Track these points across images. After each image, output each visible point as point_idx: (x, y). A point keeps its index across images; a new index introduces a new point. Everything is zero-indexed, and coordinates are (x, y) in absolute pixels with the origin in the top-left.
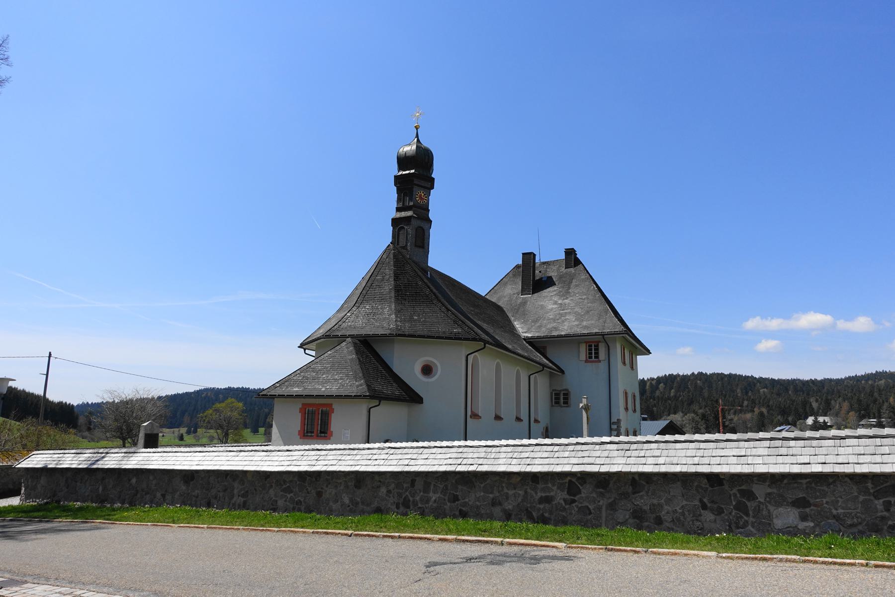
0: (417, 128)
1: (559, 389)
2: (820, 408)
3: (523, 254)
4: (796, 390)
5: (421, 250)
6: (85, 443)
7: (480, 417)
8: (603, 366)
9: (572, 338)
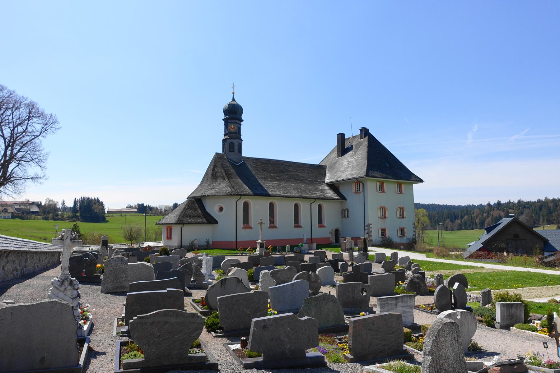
0: (233, 93)
1: (345, 209)
2: (462, 217)
3: (338, 135)
4: (447, 208)
5: (233, 153)
6: (545, 212)
7: (252, 228)
8: (362, 194)
9: (363, 178)
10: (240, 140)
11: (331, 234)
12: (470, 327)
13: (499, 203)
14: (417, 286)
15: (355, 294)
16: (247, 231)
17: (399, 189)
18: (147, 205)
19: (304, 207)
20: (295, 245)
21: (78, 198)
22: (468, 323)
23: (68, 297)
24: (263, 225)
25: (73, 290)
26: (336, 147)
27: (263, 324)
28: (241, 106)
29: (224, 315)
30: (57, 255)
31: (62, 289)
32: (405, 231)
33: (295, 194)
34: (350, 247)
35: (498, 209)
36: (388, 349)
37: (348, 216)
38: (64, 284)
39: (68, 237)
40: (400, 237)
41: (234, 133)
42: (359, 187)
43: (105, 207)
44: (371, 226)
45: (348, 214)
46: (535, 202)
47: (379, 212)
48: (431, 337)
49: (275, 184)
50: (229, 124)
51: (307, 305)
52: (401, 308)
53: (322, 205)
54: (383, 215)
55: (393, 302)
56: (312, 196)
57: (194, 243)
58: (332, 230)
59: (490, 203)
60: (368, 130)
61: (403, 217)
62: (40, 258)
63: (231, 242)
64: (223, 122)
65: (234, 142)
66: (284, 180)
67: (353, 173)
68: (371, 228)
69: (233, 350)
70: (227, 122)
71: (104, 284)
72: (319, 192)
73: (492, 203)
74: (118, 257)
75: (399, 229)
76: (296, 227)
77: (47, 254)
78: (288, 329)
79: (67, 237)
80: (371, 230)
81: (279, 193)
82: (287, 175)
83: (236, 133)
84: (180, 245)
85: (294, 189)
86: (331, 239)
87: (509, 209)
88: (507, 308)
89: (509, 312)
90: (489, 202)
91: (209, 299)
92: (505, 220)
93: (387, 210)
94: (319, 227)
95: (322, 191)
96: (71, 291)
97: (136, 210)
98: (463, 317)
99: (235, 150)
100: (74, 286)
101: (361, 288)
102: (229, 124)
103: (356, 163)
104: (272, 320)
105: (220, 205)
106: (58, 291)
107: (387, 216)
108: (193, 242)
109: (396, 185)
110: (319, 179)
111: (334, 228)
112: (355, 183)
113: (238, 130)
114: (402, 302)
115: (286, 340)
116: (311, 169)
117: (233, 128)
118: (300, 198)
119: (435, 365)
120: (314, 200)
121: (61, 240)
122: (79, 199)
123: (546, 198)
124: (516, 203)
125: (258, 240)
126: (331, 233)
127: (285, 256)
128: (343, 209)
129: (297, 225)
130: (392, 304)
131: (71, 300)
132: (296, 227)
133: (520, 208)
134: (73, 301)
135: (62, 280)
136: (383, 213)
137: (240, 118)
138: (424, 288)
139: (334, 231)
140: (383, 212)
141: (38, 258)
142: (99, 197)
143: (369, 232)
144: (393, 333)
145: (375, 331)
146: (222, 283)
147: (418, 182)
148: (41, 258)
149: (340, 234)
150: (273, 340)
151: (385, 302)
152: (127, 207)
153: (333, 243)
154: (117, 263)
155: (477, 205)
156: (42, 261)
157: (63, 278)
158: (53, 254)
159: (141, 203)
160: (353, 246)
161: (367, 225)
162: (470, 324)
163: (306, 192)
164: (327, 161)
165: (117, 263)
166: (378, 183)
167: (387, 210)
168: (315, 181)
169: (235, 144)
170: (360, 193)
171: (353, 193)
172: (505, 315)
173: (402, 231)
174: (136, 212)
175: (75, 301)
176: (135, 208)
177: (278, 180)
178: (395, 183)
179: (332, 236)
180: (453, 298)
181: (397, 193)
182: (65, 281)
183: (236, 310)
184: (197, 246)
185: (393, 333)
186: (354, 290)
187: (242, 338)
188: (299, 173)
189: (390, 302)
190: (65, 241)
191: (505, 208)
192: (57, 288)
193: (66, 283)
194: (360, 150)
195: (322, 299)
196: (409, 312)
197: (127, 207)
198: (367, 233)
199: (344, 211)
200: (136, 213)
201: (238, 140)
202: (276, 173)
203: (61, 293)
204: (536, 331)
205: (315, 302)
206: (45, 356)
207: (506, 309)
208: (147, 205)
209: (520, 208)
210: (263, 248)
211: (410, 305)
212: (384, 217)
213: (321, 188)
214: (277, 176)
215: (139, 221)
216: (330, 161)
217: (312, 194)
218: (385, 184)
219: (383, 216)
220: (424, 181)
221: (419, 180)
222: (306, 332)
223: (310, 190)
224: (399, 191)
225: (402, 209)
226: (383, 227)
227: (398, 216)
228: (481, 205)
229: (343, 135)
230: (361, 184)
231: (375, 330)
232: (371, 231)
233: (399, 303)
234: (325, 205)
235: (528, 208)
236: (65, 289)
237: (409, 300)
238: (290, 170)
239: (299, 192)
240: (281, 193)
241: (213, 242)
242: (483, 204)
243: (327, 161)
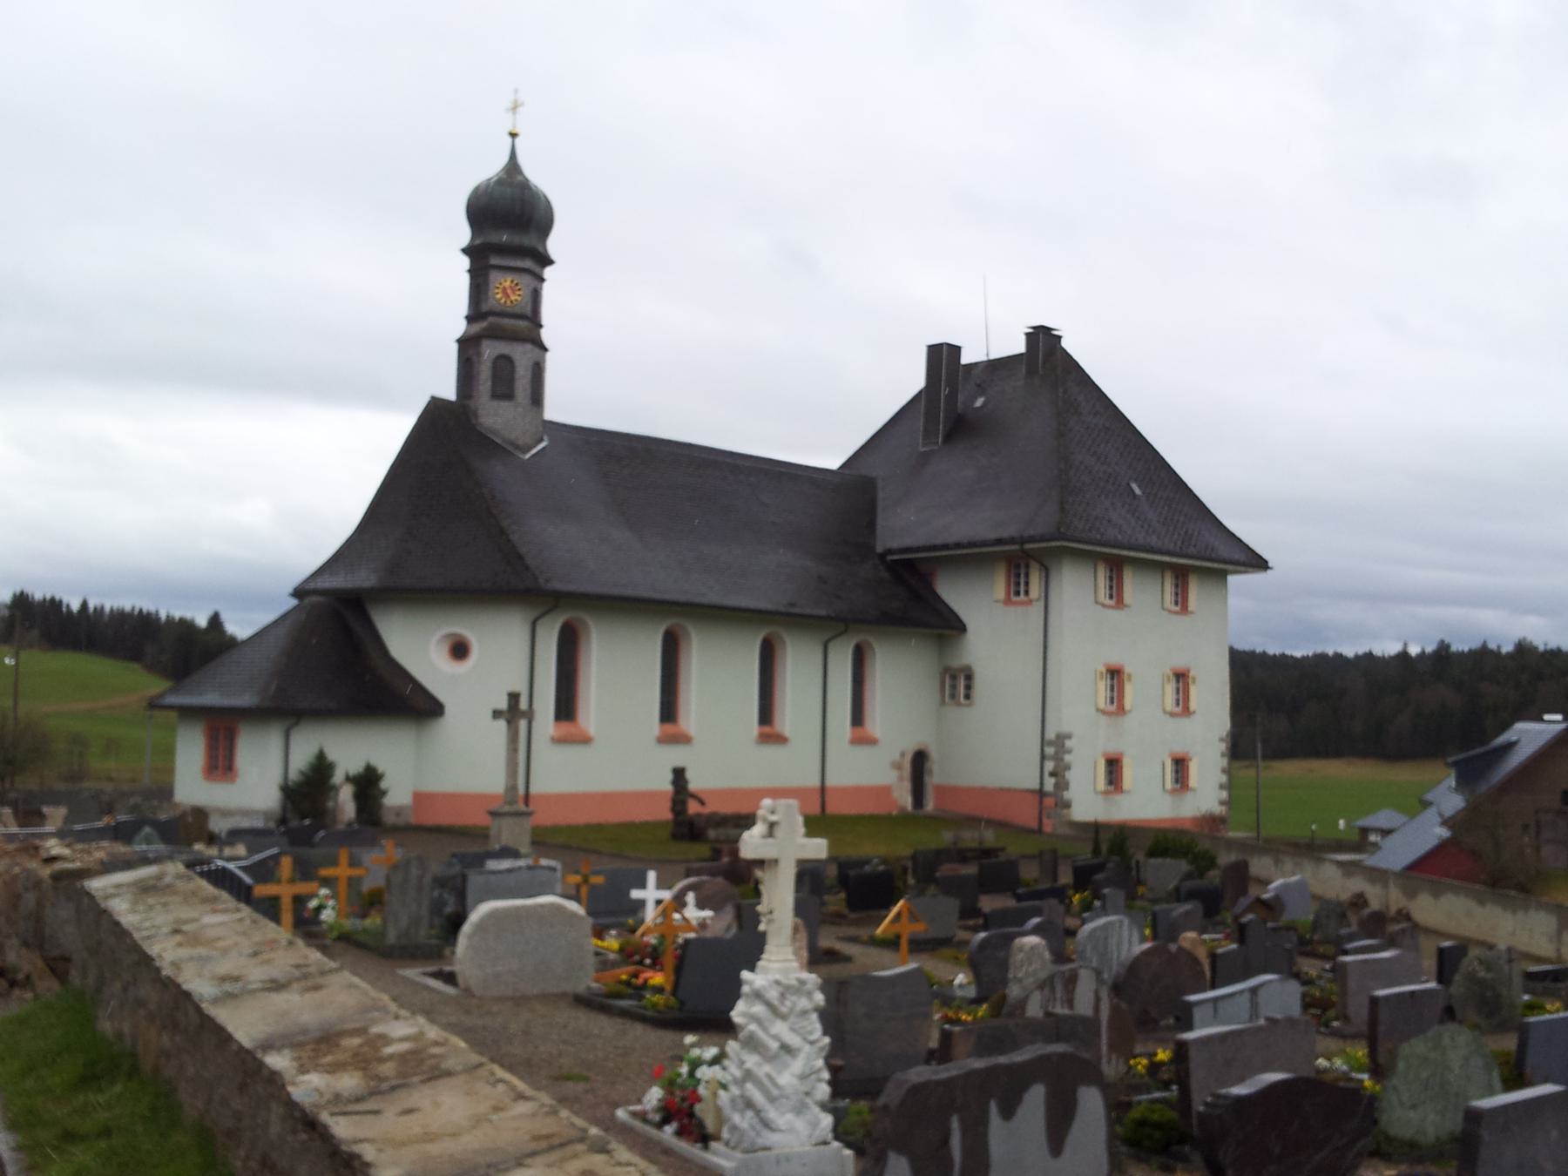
10: (537, 350)
16: (573, 753)
28: (548, 203)
37: (967, 697)
40: (1174, 791)
58: (903, 755)
60: (1059, 337)
64: (465, 262)
83: (522, 317)
86: (895, 794)
105: (460, 636)
111: (910, 745)
117: (506, 289)
137: (541, 249)
147: (1250, 570)
149: (931, 772)
167: (1194, 682)
170: (1030, 602)
171: (997, 601)
179: (901, 779)
198: (1052, 774)
201: (529, 346)
220: (1270, 565)
226: (1113, 748)
229: (955, 350)
232: (1068, 767)
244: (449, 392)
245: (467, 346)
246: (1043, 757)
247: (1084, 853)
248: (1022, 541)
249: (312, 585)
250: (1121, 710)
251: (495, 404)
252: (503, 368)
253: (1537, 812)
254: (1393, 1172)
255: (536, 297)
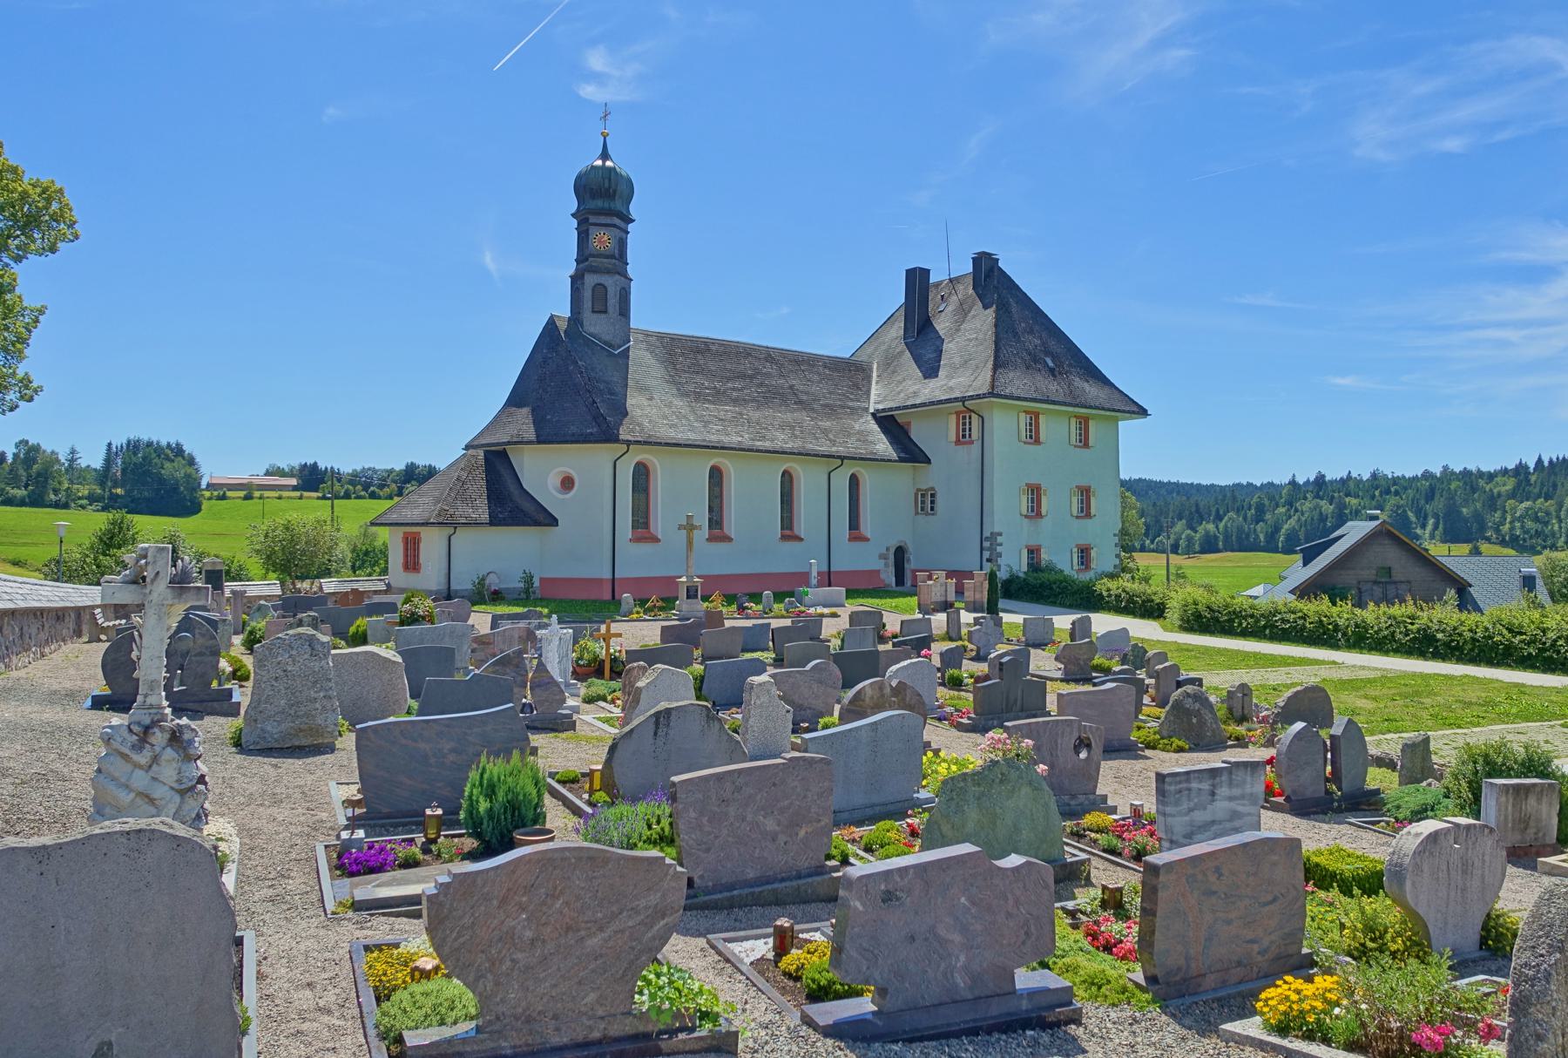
2: (1219, 518)
5: (603, 316)
11: (883, 561)
12: (1487, 872)
13: (1320, 481)
14: (1194, 720)
15: (1057, 755)
17: (1080, 434)
18: (326, 468)
19: (809, 481)
20: (787, 588)
21: (119, 440)
22: (1484, 861)
23: (167, 788)
24: (695, 531)
25: (183, 760)
26: (903, 309)
27: (883, 887)
29: (693, 836)
30: (73, 615)
31: (143, 758)
32: (1093, 553)
33: (786, 443)
34: (943, 599)
35: (1317, 496)
36: (1259, 953)
37: (932, 509)
38: (152, 740)
39: (161, 574)
41: (607, 257)
42: (967, 427)
43: (203, 470)
44: (999, 539)
45: (932, 502)
46: (1415, 478)
47: (1024, 499)
48: (1543, 952)
49: (727, 411)
50: (592, 230)
51: (952, 799)
52: (1226, 804)
53: (859, 477)
54: (1032, 507)
55: (1206, 786)
56: (834, 449)
57: (487, 582)
58: (888, 549)
59: (1297, 480)
60: (998, 260)
61: (1088, 515)
62: (22, 629)
63: (597, 582)
64: (575, 223)
65: (606, 284)
66: (754, 400)
67: (951, 384)
68: (1001, 545)
69: (752, 963)
70: (584, 221)
71: (256, 721)
72: (854, 439)
73: (1301, 480)
74: (299, 634)
75: (1075, 550)
76: (784, 538)
77: (42, 614)
78: (963, 900)
79: (158, 573)
80: (999, 549)
81: (740, 439)
82: (761, 385)
83: (612, 257)
84: (443, 587)
85: (781, 428)
86: (883, 576)
87: (1347, 495)
88: (1514, 799)
89: (1521, 808)
90: (1294, 476)
91: (616, 775)
92: (1353, 527)
93: (1045, 495)
94: (850, 540)
95: (863, 436)
96: (175, 765)
97: (294, 482)
98: (1470, 843)
99: (610, 309)
100: (185, 749)
101: (1076, 735)
102: (592, 230)
103: (961, 356)
104: (911, 871)
106: (129, 767)
107: (1044, 513)
108: (483, 579)
109: (1073, 421)
110: (852, 400)
111: (893, 543)
112: (958, 413)
113: (617, 247)
114: (1231, 784)
115: (957, 938)
116: (829, 369)
117: (602, 240)
118: (800, 454)
119: (1560, 1049)
120: (839, 461)
121: (135, 582)
122: (122, 446)
123: (1446, 468)
124: (1365, 479)
125: (680, 577)
126: (883, 557)
127: (770, 624)
128: (918, 490)
129: (787, 532)
130: (1200, 789)
131: (177, 798)
132: (784, 538)
133: (1377, 493)
134: (182, 802)
135: (143, 726)
136: (1033, 502)
138: (1214, 726)
139: (892, 551)
140: (1032, 499)
141: (17, 629)
142: (181, 441)
143: (994, 557)
144: (1275, 900)
145: (1223, 896)
146: (657, 723)
148: (25, 628)
149: (909, 560)
150: (914, 940)
151: (1181, 786)
152: (267, 470)
153: (889, 586)
154: (294, 652)
155: (1259, 485)
156: (30, 638)
157: (147, 721)
158: (60, 613)
159: (310, 461)
160: (951, 597)
161: (989, 535)
162: (1487, 864)
163: (817, 439)
164: (876, 349)
165: (294, 652)
166: (1022, 416)
167: (1045, 495)
168: (842, 407)
169: (609, 289)
170: (972, 442)
172: (1510, 817)
173: (1084, 553)
174: (295, 488)
175: (191, 801)
176: (291, 474)
177: (735, 401)
178: (1070, 416)
179: (886, 565)
180: (1329, 762)
181: (1075, 446)
182: (151, 731)
183: (732, 820)
184: (1522, 750)
185: (1275, 900)
186: (1056, 742)
187: (778, 923)
188: (794, 382)
189: (1194, 785)
190: (149, 587)
191: (1336, 495)
192: (125, 757)
193: (159, 738)
194: (974, 316)
195: (998, 780)
196: (1249, 814)
197: (268, 473)
199: (923, 496)
200: (293, 490)
201: (617, 277)
202: (729, 379)
203: (139, 773)
204: (624, 656)
205: (977, 789)
206: (113, 1039)
207: (1511, 800)
208: (326, 468)
209: (1377, 493)
210: (694, 601)
211: (1251, 794)
212: (1037, 514)
213: (857, 427)
214: (734, 389)
215: (309, 512)
216: (883, 348)
217: (833, 443)
218: (1091, 423)
219: (1033, 511)
221: (1135, 409)
222: (1018, 909)
223: (825, 432)
224: (1080, 441)
225: (1085, 493)
226: (1033, 542)
227: (1075, 513)
228: (1271, 484)
229: (925, 273)
230: (973, 415)
231: (1225, 894)
232: (1000, 555)
233: (1221, 787)
234: (868, 478)
235: (1397, 493)
236: (155, 759)
237: (1249, 779)
238: (770, 374)
239: (796, 437)
240: (745, 439)
241: (542, 580)
242: (1277, 482)
243: (876, 349)
244: (564, 311)
245: (576, 280)
246: (982, 549)
247: (1359, 622)
248: (963, 400)
249: (476, 443)
250: (1039, 515)
251: (595, 316)
252: (600, 292)
253: (1359, 582)
254: (571, 1056)
255: (622, 244)
